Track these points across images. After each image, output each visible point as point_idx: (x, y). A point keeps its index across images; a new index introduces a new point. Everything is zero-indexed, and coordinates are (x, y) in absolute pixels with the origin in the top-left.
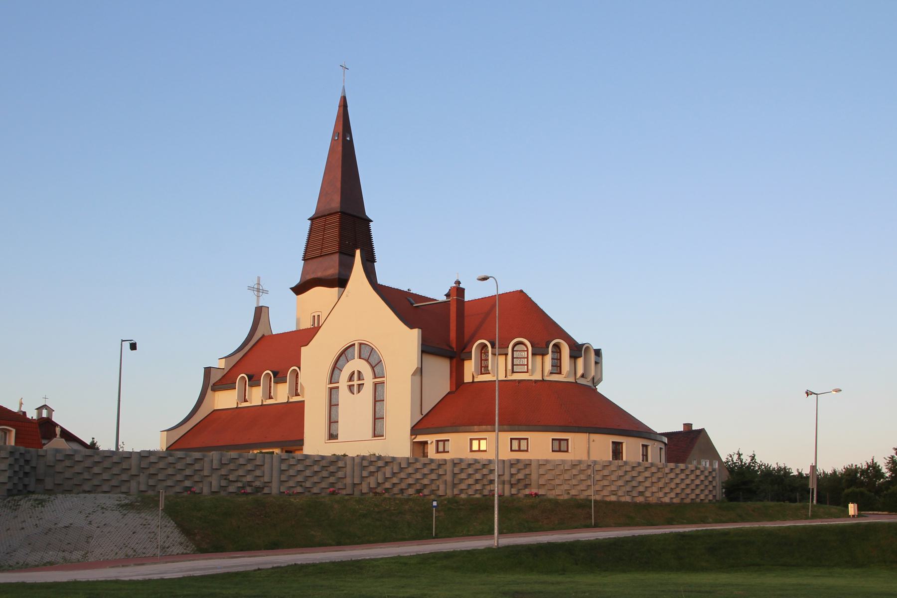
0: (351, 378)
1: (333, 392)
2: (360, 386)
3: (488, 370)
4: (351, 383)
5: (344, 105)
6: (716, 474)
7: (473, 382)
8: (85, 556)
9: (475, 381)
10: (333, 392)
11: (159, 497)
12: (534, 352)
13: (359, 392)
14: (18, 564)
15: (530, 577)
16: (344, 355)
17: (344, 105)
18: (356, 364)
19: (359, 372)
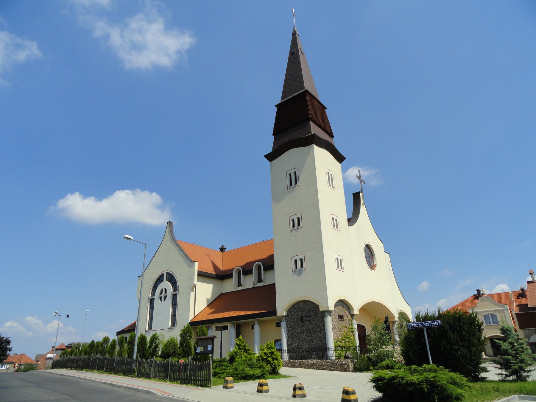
0: (161, 293)
1: (152, 301)
2: (165, 297)
3: (262, 280)
4: (161, 296)
5: (294, 34)
6: (420, 323)
7: (254, 287)
8: (359, 356)
9: (255, 286)
10: (152, 301)
11: (496, 324)
12: (199, 274)
13: (165, 300)
14: (380, 356)
15: (506, 357)
16: (160, 280)
17: (294, 34)
18: (166, 285)
19: (166, 290)
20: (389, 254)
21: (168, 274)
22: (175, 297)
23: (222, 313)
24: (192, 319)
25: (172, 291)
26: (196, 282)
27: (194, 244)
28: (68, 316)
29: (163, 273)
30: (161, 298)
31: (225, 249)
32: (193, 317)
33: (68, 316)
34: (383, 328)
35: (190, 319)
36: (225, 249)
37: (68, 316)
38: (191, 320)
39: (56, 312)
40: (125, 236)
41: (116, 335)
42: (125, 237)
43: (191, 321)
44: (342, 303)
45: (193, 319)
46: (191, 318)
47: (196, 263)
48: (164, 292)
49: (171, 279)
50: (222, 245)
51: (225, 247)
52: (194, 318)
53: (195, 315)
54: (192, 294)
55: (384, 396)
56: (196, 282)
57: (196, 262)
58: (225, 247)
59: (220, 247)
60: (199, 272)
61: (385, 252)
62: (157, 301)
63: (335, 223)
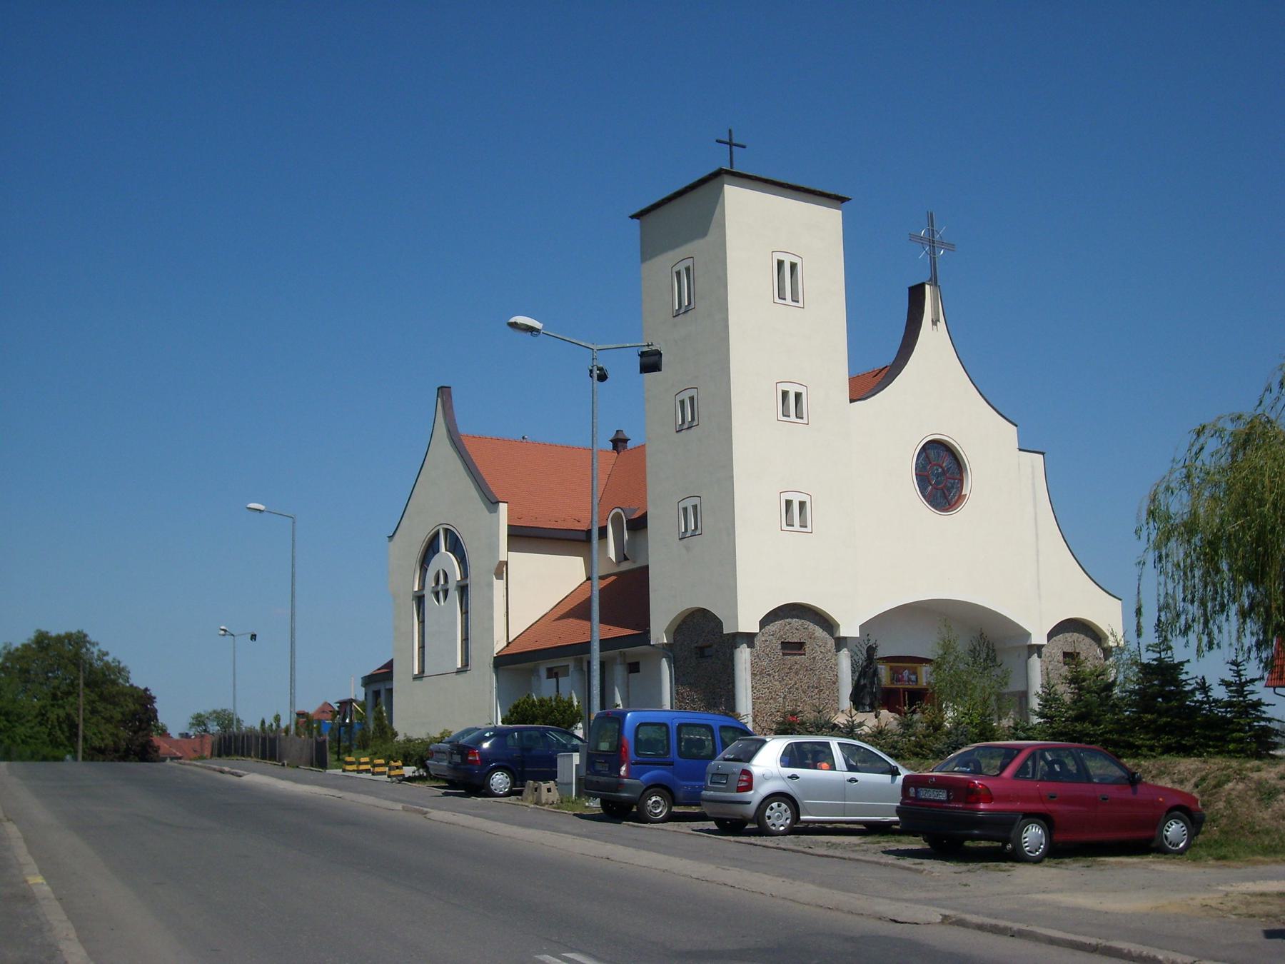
1: (420, 599)
2: (446, 592)
16: (431, 548)
18: (445, 560)
20: (1043, 454)
21: (446, 530)
22: (463, 590)
23: (612, 628)
24: (502, 650)
25: (459, 578)
26: (503, 554)
27: (523, 438)
28: (254, 637)
29: (436, 529)
30: (437, 595)
31: (626, 441)
32: (505, 644)
33: (254, 637)
34: (681, 706)
35: (497, 649)
36: (626, 441)
37: (255, 635)
38: (499, 652)
39: (222, 628)
40: (512, 320)
41: (360, 684)
42: (514, 325)
43: (500, 654)
44: (181, 735)
45: (504, 648)
46: (499, 645)
47: (503, 508)
48: (442, 582)
49: (456, 547)
50: (617, 431)
51: (627, 434)
52: (507, 646)
53: (510, 640)
54: (499, 585)
55: (963, 842)
56: (503, 554)
57: (500, 504)
58: (628, 437)
59: (612, 436)
60: (510, 527)
61: (1020, 450)
62: (430, 599)
63: (793, 404)
